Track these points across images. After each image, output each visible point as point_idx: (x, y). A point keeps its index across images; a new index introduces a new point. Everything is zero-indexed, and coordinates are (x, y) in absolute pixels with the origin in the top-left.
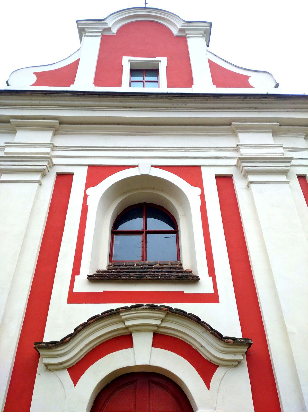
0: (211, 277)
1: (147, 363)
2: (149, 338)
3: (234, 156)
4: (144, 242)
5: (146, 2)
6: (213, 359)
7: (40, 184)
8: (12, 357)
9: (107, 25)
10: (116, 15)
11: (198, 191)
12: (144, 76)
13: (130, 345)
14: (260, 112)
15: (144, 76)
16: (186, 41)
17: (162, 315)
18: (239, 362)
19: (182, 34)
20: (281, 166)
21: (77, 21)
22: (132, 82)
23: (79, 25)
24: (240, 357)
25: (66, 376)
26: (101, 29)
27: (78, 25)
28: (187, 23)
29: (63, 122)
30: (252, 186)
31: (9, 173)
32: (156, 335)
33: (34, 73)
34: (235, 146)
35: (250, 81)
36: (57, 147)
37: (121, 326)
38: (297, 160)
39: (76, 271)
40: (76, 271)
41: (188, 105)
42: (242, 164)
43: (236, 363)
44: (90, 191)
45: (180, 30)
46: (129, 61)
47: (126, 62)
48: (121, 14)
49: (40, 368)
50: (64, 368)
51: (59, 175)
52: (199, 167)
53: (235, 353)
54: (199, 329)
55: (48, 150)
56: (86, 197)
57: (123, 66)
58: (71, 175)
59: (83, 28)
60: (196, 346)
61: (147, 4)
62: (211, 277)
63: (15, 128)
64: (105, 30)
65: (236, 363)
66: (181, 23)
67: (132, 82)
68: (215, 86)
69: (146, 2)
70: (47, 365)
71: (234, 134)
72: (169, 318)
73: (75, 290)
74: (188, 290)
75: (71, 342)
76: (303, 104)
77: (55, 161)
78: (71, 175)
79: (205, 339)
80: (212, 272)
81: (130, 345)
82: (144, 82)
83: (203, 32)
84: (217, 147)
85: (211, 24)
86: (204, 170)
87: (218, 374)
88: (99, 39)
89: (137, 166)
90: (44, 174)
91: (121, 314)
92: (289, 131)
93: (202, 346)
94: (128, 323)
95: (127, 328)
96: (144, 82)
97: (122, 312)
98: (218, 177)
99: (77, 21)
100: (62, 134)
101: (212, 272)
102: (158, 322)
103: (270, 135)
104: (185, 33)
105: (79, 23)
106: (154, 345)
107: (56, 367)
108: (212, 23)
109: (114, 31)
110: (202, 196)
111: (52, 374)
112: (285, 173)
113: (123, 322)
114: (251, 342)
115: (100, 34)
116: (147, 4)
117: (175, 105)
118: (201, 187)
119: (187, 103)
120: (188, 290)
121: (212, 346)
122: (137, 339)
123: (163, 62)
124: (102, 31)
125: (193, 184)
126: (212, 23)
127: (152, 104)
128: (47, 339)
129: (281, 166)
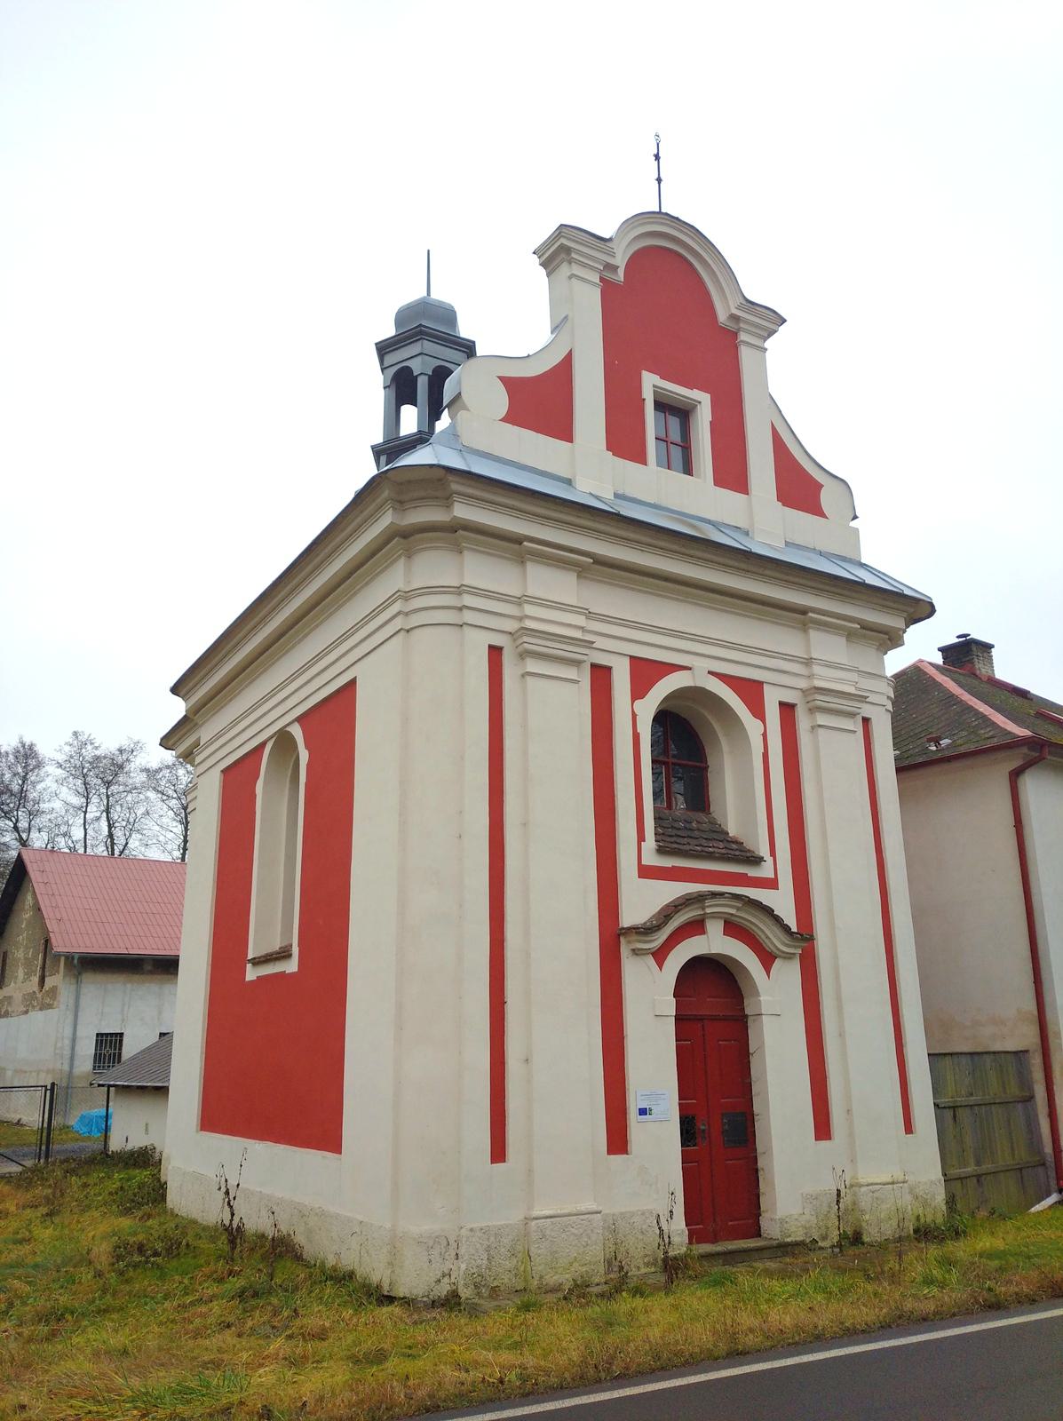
8: (904, 1005)
19: (731, 326)
25: (651, 961)
26: (600, 264)
30: (821, 731)
31: (545, 660)
41: (767, 572)
47: (650, 382)
52: (760, 684)
54: (769, 921)
56: (634, 716)
57: (644, 400)
58: (609, 669)
59: (739, 317)
71: (804, 627)
73: (643, 863)
74: (752, 872)
76: (895, 602)
78: (609, 669)
79: (772, 931)
80: (773, 853)
84: (786, 655)
86: (767, 689)
87: (778, 963)
98: (781, 704)
101: (773, 853)
102: (733, 911)
103: (844, 640)
105: (564, 230)
111: (638, 958)
112: (577, 663)
117: (751, 568)
119: (765, 568)
120: (752, 872)
121: (779, 939)
124: (602, 268)
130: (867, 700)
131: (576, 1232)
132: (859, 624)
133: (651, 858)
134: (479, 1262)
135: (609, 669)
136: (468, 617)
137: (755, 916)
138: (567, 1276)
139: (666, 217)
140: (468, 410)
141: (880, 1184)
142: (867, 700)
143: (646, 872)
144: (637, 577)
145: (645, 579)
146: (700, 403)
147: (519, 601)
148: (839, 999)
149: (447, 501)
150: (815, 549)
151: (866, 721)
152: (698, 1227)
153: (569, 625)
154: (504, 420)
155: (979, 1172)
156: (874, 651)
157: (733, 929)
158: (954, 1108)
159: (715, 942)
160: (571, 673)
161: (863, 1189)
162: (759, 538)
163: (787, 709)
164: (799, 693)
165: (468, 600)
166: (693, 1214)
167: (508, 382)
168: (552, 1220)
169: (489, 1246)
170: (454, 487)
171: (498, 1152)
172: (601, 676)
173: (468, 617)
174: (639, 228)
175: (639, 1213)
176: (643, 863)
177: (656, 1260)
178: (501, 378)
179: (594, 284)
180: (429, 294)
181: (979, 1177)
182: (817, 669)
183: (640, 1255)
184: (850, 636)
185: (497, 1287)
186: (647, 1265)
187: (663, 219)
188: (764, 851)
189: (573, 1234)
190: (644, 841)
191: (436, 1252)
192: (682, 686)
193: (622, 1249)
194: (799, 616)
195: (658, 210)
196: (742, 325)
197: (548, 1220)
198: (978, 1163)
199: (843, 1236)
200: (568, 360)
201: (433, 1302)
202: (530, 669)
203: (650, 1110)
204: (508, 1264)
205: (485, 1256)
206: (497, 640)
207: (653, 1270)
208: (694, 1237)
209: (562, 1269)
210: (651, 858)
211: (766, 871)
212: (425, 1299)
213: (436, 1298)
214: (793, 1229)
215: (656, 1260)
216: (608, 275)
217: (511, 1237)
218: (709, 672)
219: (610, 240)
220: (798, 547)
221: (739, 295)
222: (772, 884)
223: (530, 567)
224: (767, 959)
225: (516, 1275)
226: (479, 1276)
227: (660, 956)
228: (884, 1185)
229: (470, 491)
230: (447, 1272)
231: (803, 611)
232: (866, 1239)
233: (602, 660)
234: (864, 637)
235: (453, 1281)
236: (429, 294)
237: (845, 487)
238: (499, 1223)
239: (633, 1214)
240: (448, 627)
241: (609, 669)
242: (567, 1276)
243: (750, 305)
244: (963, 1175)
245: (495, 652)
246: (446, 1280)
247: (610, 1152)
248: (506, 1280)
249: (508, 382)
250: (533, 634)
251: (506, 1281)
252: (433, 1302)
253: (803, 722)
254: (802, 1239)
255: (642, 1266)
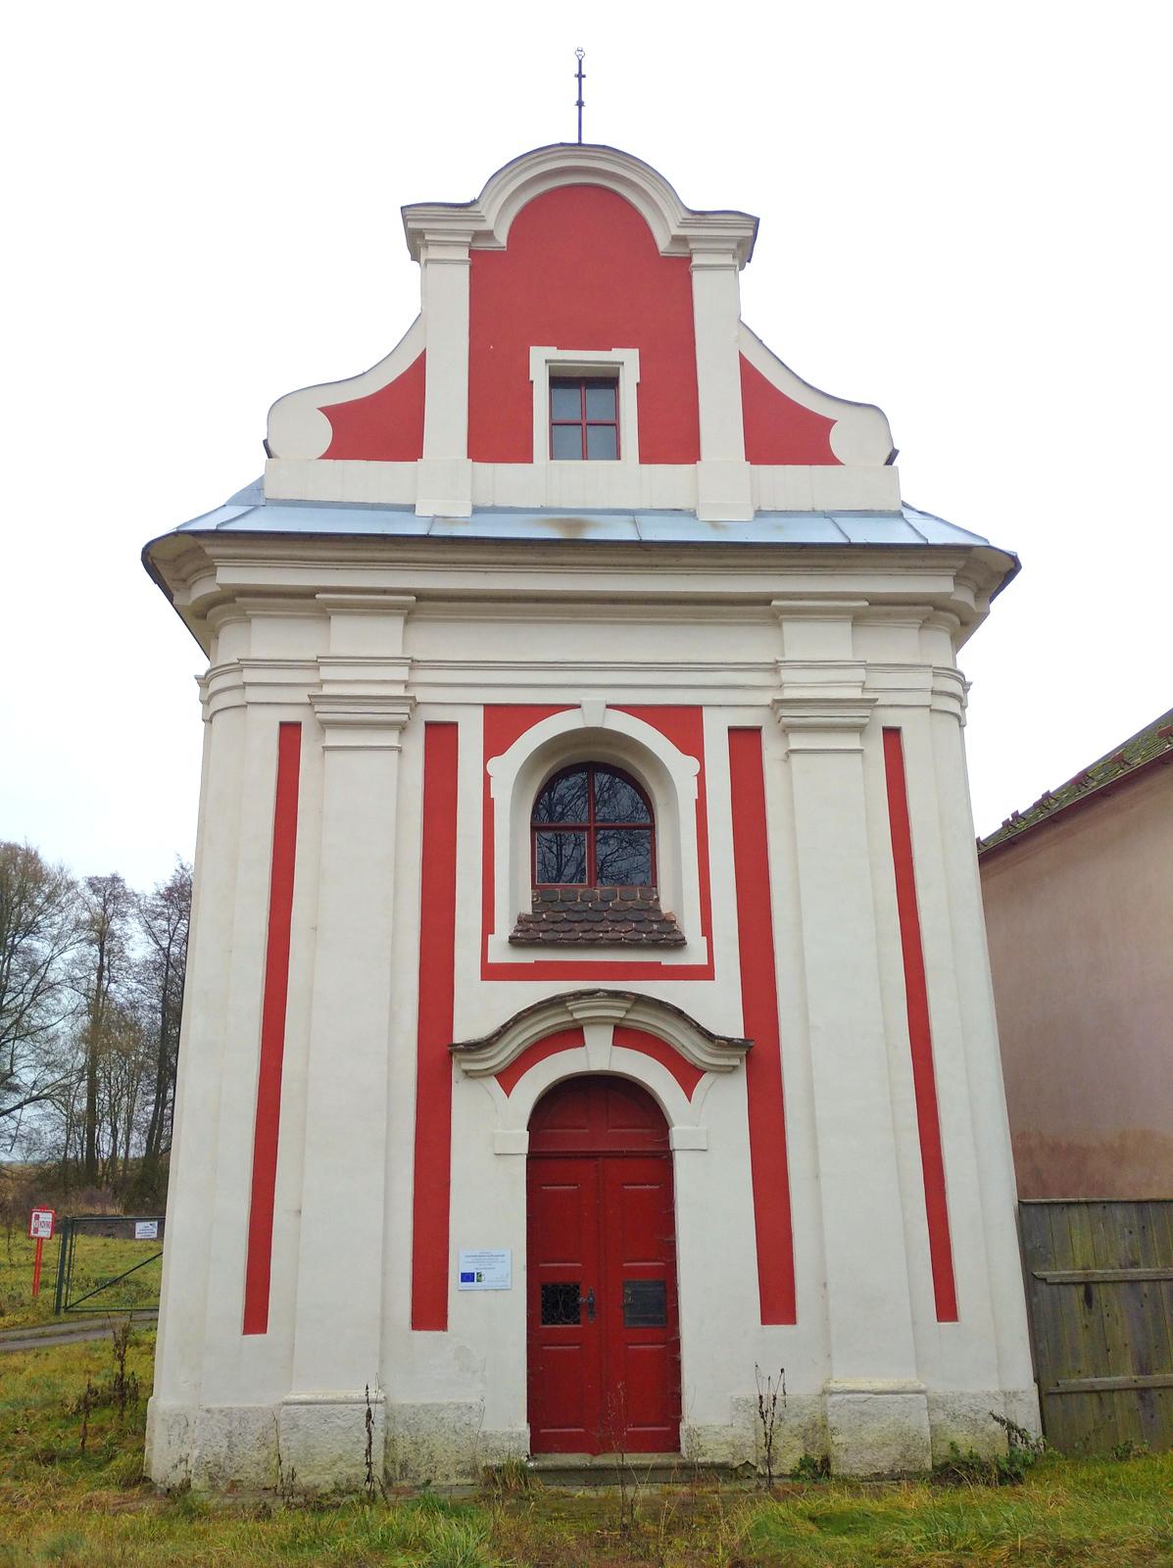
0: (705, 938)
1: (606, 1067)
2: (608, 1033)
3: (768, 683)
4: (583, 413)
5: (580, 71)
6: (698, 1063)
7: (400, 750)
9: (482, 220)
10: (506, 175)
11: (692, 763)
12: (583, 389)
13: (581, 1043)
14: (832, 575)
15: (583, 389)
16: (689, 277)
17: (628, 1005)
18: (735, 1067)
19: (679, 251)
20: (853, 716)
21: (402, 208)
22: (553, 424)
23: (408, 220)
24: (735, 1062)
25: (494, 1084)
27: (405, 221)
28: (694, 217)
29: (422, 596)
30: (794, 758)
31: (800, 732)
32: (616, 1028)
33: (321, 409)
34: (772, 661)
35: (837, 441)
36: (419, 661)
37: (567, 1018)
38: (892, 694)
39: (488, 927)
40: (488, 927)
41: (685, 561)
42: (781, 710)
43: (731, 1069)
44: (494, 763)
45: (677, 240)
46: (546, 361)
47: (541, 360)
48: (518, 170)
49: (456, 1073)
50: (491, 1074)
51: (430, 726)
52: (700, 708)
53: (729, 1057)
54: (682, 1025)
55: (402, 673)
56: (487, 778)
57: (532, 382)
58: (453, 726)
59: (421, 229)
60: (677, 1046)
61: (584, 76)
62: (705, 938)
63: (326, 612)
64: (478, 235)
65: (731, 1069)
66: (679, 216)
67: (553, 424)
68: (749, 463)
69: (580, 71)
70: (466, 1072)
71: (775, 619)
72: (638, 1008)
73: (491, 960)
74: (668, 959)
75: (499, 1042)
77: (421, 695)
78: (453, 726)
80: (707, 930)
81: (581, 1043)
82: (584, 425)
83: (734, 246)
85: (755, 222)
86: (706, 713)
88: (462, 275)
89: (579, 707)
90: (402, 728)
91: (568, 1004)
92: (888, 615)
93: (683, 1046)
94: (577, 1016)
95: (575, 1020)
96: (584, 425)
97: (570, 1001)
98: (733, 732)
99: (402, 208)
100: (420, 620)
101: (707, 930)
102: (621, 1014)
104: (687, 245)
105: (407, 213)
106: (614, 1044)
107: (481, 1074)
108: (759, 219)
109: (502, 239)
110: (701, 777)
112: (859, 729)
113: (571, 1013)
114: (751, 1044)
115: (464, 254)
116: (584, 76)
117: (655, 561)
118: (700, 757)
120: (668, 959)
122: (589, 1034)
123: (628, 362)
124: (470, 240)
125: (686, 751)
126: (759, 219)
127: (608, 560)
128: (461, 1034)
129: (853, 716)
130: (877, 703)
131: (342, 1424)
132: (867, 600)
133: (501, 952)
134: (217, 1449)
135: (455, 725)
136: (252, 695)
137: (663, 1020)
138: (327, 1477)
139: (562, 148)
140: (324, 457)
141: (869, 1392)
142: (877, 703)
143: (491, 972)
144: (594, 606)
145: (589, 606)
146: (623, 363)
147: (775, 667)
148: (813, 1125)
149: (210, 569)
150: (814, 511)
151: (892, 735)
152: (578, 1430)
153: (384, 682)
154: (330, 455)
155: (1141, 1384)
156: (914, 633)
157: (625, 1036)
158: (1088, 1286)
159: (599, 1054)
160: (852, 742)
161: (835, 1398)
162: (704, 516)
163: (745, 742)
164: (766, 712)
165: (250, 676)
166: (538, 1411)
167: (330, 412)
168: (309, 1407)
169: (230, 1432)
170: (209, 551)
171: (256, 1318)
172: (441, 739)
173: (252, 695)
174: (523, 175)
175: (452, 1406)
176: (491, 960)
177: (475, 1468)
178: (321, 409)
179: (461, 262)
180: (580, 138)
181: (1143, 1392)
182: (787, 675)
183: (990, 1444)
184: (858, 619)
185: (240, 1481)
186: (462, 1473)
187: (560, 151)
188: (690, 925)
189: (339, 1426)
190: (493, 933)
191: (175, 1432)
192: (556, 734)
193: (423, 1450)
194: (760, 609)
195: (577, 142)
196: (692, 246)
197: (304, 1407)
198: (1144, 1369)
199: (806, 1463)
200: (420, 365)
201: (168, 1490)
202: (793, 746)
203: (480, 1275)
204: (256, 1456)
205: (225, 1443)
206: (291, 715)
207: (470, 1481)
208: (539, 1444)
209: (319, 1468)
210: (501, 952)
211: (695, 953)
212: (162, 1486)
213: (171, 1485)
214: (711, 1446)
215: (475, 1468)
216: (482, 245)
217: (261, 1424)
218: (608, 707)
219: (474, 203)
220: (494, 510)
221: (680, 208)
222: (706, 973)
223: (787, 627)
224: (688, 1076)
225: (266, 1470)
226: (216, 1465)
227: (508, 1078)
228: (876, 1393)
229: (230, 551)
230: (184, 1457)
231: (765, 600)
232: (834, 1470)
233: (892, 719)
234: (878, 616)
235: (189, 1468)
236: (580, 138)
237: (282, 401)
238: (247, 1405)
239: (441, 1408)
240: (233, 711)
241: (455, 725)
242: (327, 1477)
243: (698, 216)
244: (1098, 1388)
245: (290, 734)
246: (182, 1466)
247: (940, 1319)
248: (251, 1474)
249: (330, 412)
250: (352, 701)
251: (253, 1475)
252: (168, 1490)
253: (771, 751)
254: (726, 1460)
255: (452, 1473)
